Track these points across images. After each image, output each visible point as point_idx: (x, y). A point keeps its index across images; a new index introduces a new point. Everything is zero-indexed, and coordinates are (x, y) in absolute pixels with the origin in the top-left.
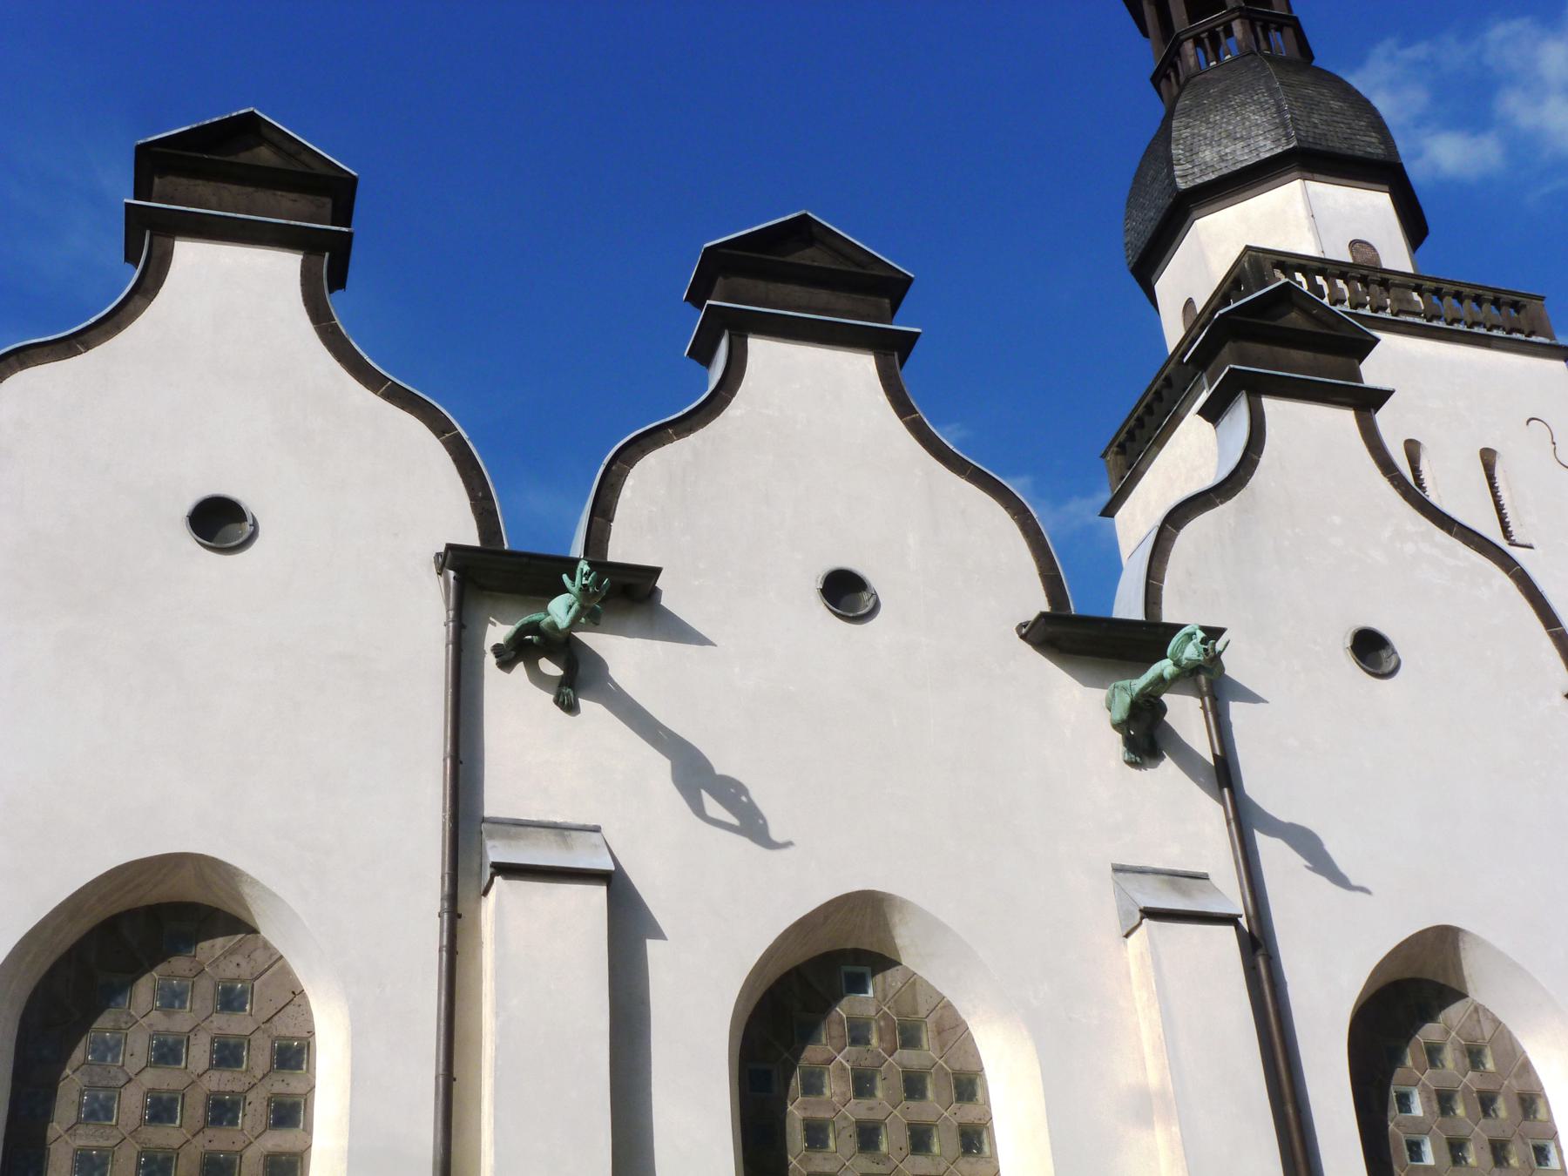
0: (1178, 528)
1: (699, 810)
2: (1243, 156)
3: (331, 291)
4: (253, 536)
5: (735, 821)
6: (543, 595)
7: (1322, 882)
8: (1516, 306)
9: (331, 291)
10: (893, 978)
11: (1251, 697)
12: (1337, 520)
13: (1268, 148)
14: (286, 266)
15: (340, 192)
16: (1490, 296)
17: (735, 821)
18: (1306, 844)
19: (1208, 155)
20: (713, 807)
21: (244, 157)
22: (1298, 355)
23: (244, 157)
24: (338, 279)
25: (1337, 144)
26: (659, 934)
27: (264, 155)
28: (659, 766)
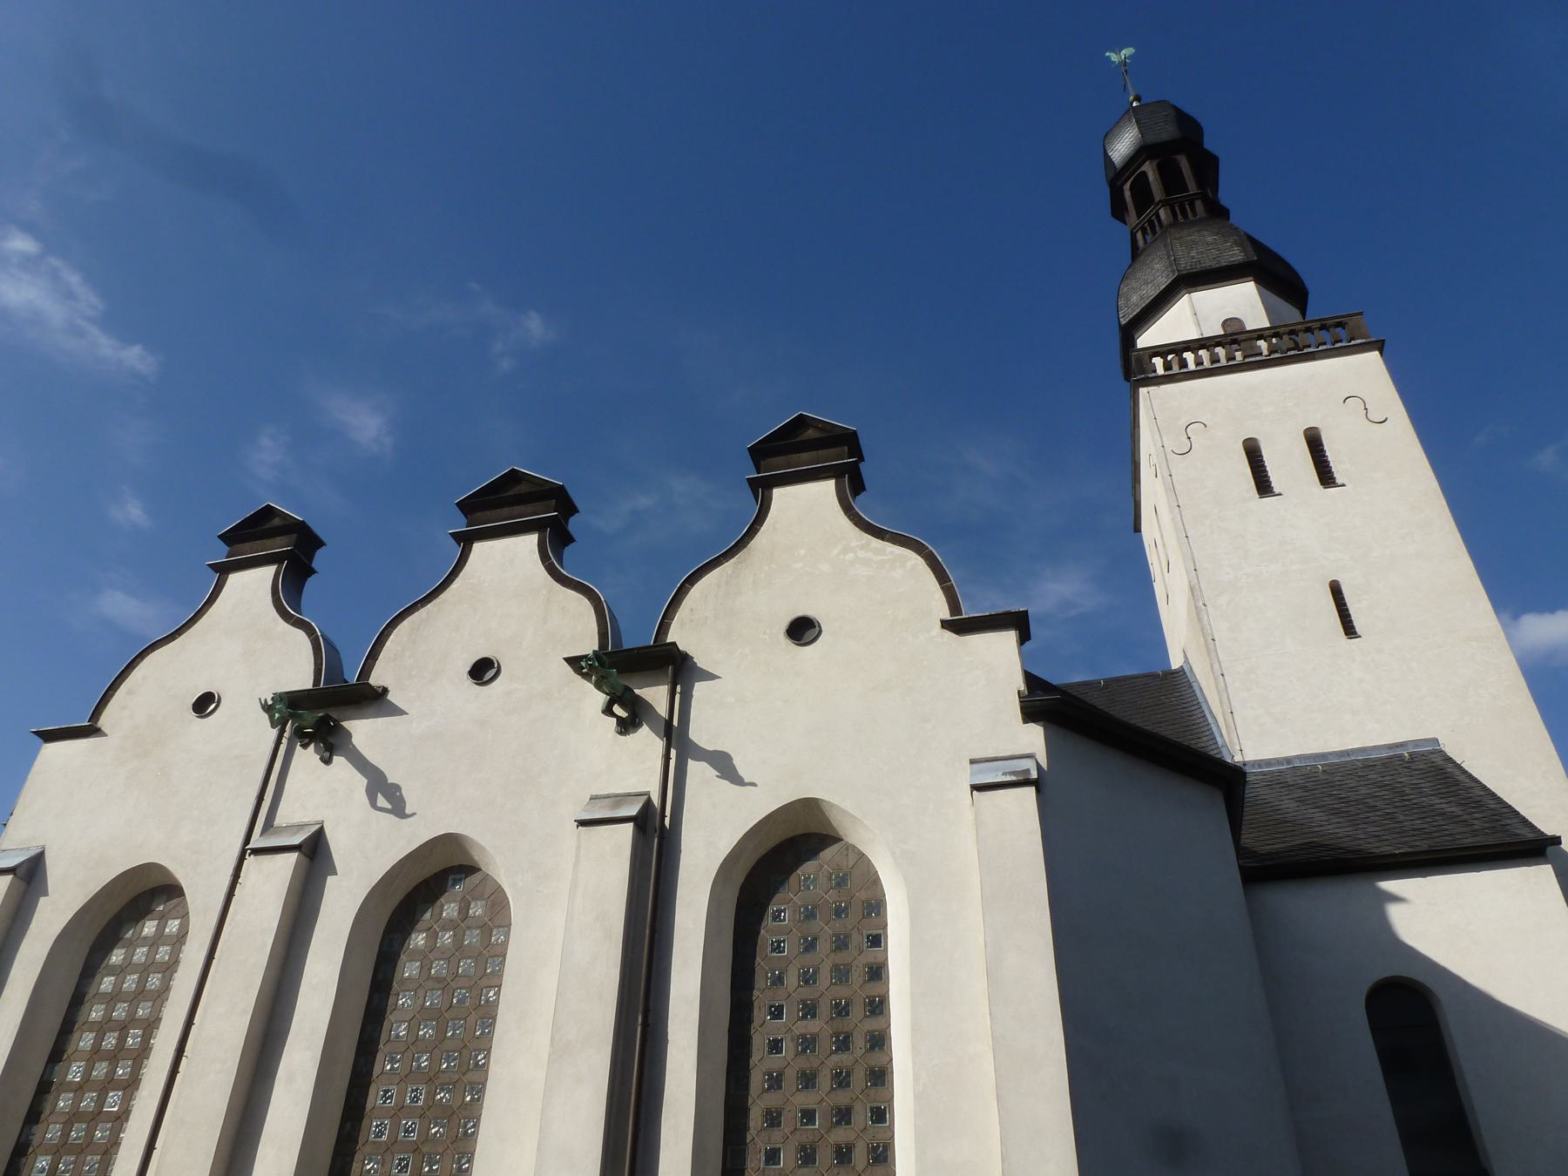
0: (692, 585)
1: (373, 804)
2: (1151, 292)
3: (854, 497)
4: (820, 632)
5: (389, 806)
6: (637, 669)
7: (725, 784)
8: (1340, 325)
9: (854, 497)
10: (474, 879)
11: (711, 677)
12: (802, 552)
13: (1163, 282)
14: (826, 489)
15: (850, 441)
16: (1318, 325)
17: (389, 806)
18: (723, 765)
19: (1135, 298)
20: (382, 801)
21: (268, 526)
22: (805, 456)
23: (268, 526)
24: (858, 486)
25: (1209, 263)
26: (46, 894)
27: (811, 433)
28: (361, 782)
